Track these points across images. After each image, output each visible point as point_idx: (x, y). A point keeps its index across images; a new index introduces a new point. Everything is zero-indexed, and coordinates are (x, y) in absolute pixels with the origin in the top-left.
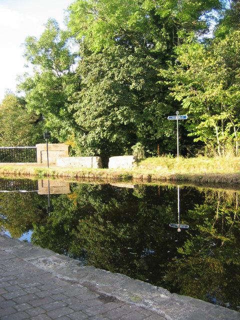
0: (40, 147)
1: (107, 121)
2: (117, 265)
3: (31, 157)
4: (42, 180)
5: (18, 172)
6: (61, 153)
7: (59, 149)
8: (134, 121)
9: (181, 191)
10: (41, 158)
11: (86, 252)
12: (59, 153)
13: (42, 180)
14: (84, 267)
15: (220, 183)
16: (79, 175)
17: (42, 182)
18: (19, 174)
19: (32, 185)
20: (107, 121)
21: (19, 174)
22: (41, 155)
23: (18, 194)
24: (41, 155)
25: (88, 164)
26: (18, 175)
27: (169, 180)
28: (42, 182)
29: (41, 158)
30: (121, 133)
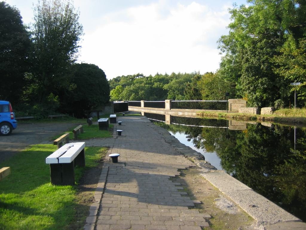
0: (230, 101)
1: (252, 86)
2: (175, 154)
3: (224, 106)
4: (231, 121)
5: (211, 115)
6: (242, 105)
7: (241, 102)
8: (266, 87)
9: (296, 129)
10: (231, 108)
11: (246, 164)
12: (241, 105)
13: (231, 121)
14: (30, 122)
15: (287, 122)
16: (235, 117)
17: (231, 122)
18: (212, 116)
19: (224, 123)
20: (251, 87)
21: (212, 116)
22: (231, 106)
23: (218, 129)
24: (231, 106)
25: (252, 111)
26: (211, 117)
27: (271, 120)
28: (231, 122)
29: (231, 108)
30: (269, 94)
